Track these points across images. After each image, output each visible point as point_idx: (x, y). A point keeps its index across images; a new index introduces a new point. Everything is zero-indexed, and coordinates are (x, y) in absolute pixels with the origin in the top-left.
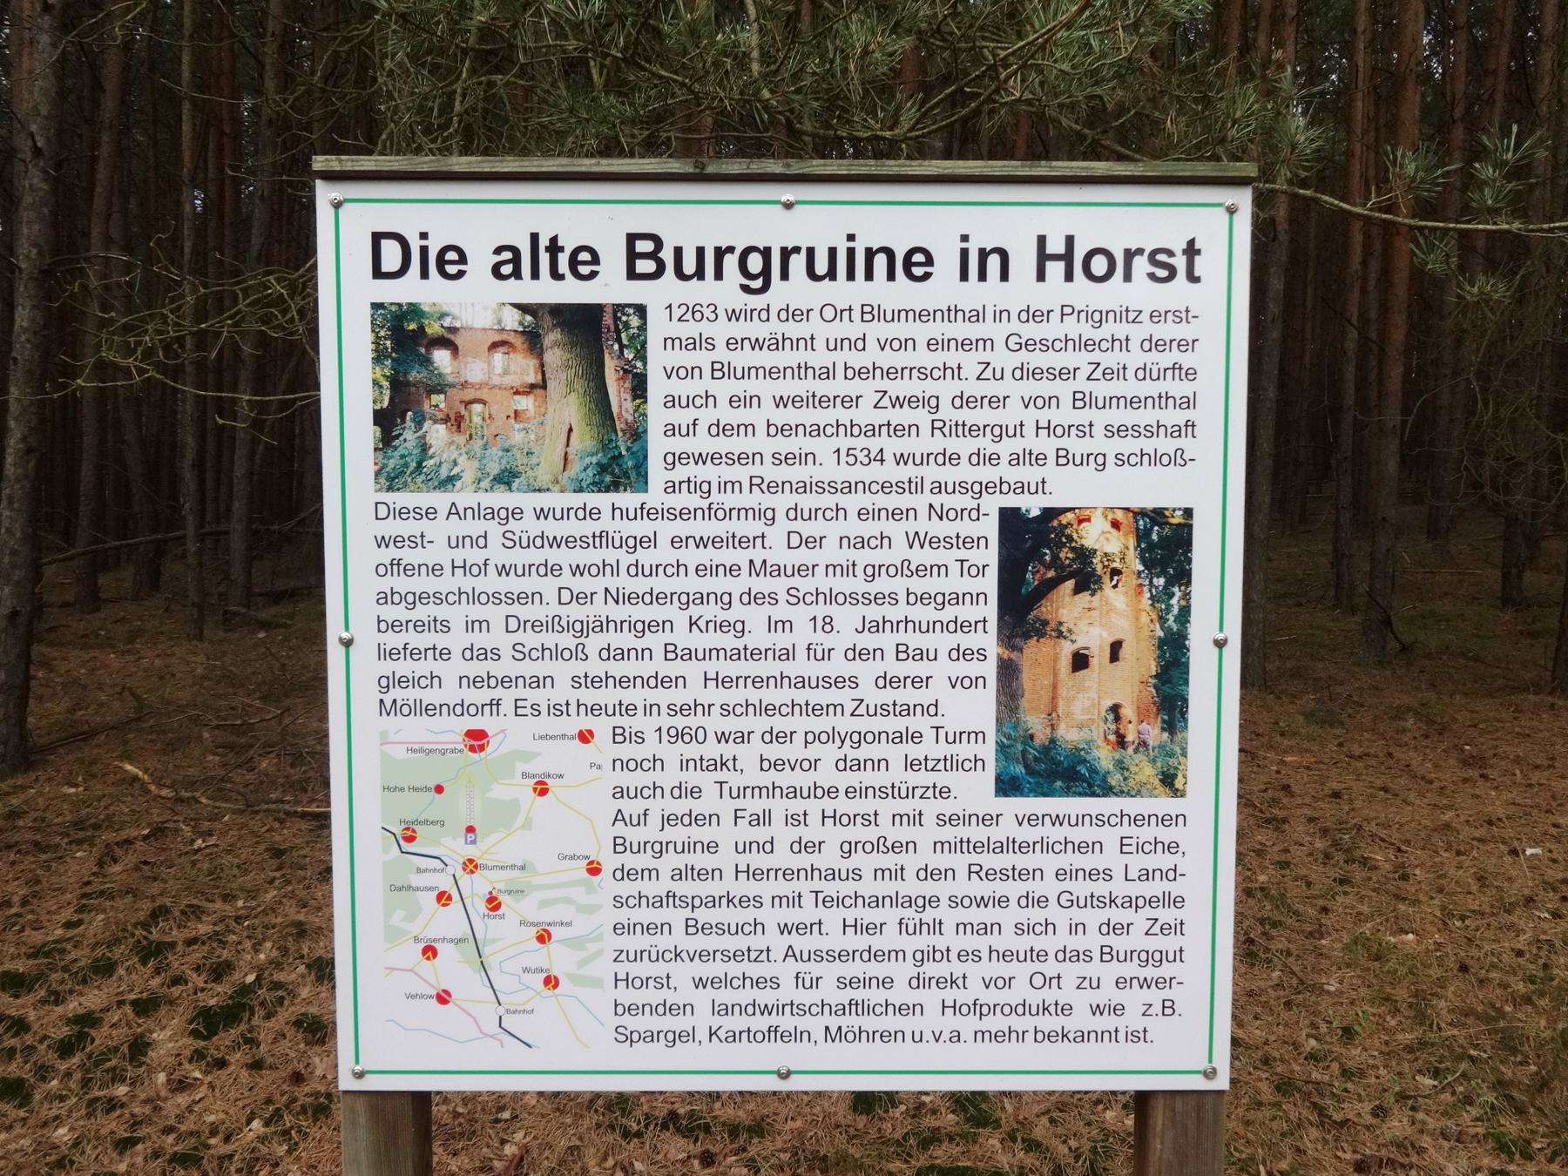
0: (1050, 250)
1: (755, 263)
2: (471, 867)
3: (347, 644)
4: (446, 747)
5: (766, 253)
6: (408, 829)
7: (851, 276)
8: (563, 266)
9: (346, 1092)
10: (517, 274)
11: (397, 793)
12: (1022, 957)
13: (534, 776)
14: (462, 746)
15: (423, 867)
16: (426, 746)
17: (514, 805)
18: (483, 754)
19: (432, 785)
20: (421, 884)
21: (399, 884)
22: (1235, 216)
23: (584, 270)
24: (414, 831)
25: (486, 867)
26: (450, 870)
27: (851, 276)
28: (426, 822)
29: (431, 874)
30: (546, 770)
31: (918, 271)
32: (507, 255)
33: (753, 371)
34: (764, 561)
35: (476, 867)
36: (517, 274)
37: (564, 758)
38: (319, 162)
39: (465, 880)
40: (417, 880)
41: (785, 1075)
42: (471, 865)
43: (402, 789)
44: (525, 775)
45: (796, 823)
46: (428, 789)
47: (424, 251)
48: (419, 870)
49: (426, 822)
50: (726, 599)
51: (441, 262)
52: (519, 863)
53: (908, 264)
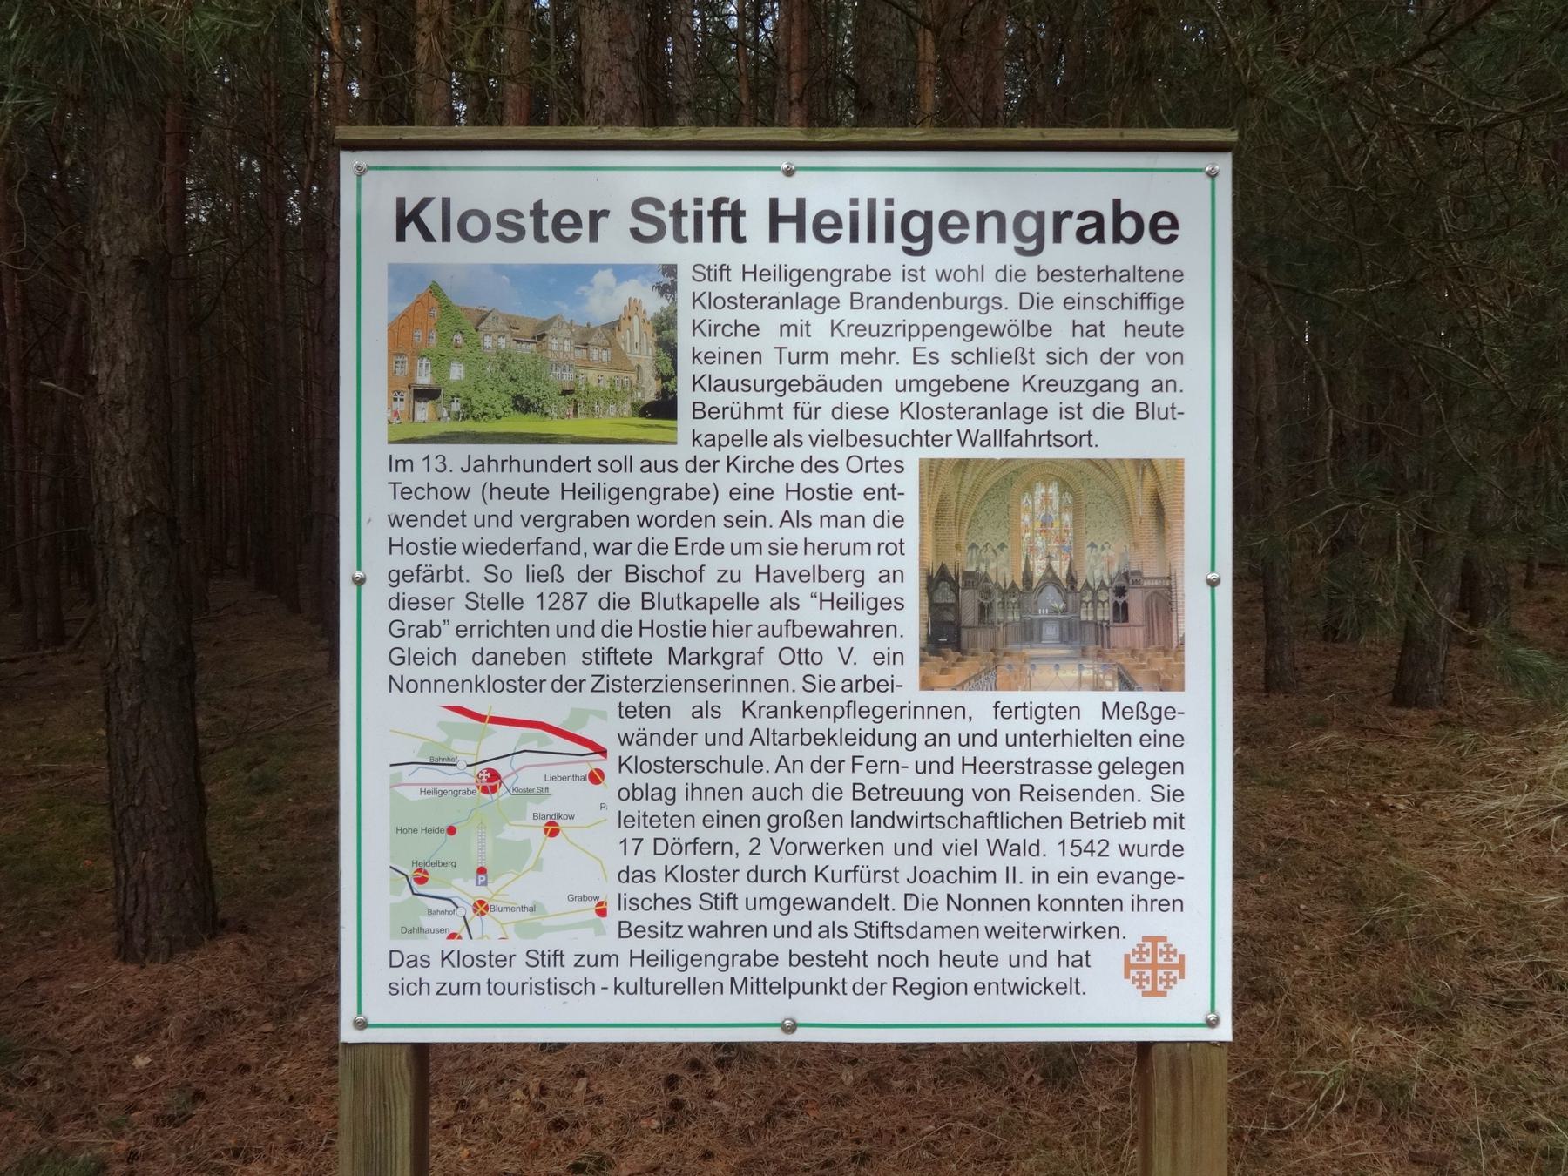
0: (782, 212)
1: (917, 226)
2: (481, 909)
3: (359, 582)
4: (458, 788)
5: (927, 217)
6: (419, 870)
7: (872, 238)
8: (547, 229)
9: (346, 1044)
10: (1100, 237)
11: (410, 835)
12: (972, 962)
13: (545, 817)
14: (475, 788)
15: (434, 909)
16: (440, 788)
17: (525, 846)
18: (495, 795)
19: (445, 826)
20: (432, 926)
21: (410, 926)
22: (1217, 179)
23: (567, 233)
24: (426, 872)
25: (497, 909)
26: (461, 912)
27: (872, 238)
28: (438, 863)
29: (442, 916)
30: (557, 811)
31: (1164, 234)
32: (1091, 220)
33: (914, 384)
34: (684, 649)
35: (486, 908)
36: (1100, 237)
37: (575, 798)
38: (343, 132)
39: (475, 922)
40: (428, 922)
41: (792, 1028)
42: (481, 907)
43: (415, 831)
44: (536, 816)
45: (617, 689)
46: (441, 831)
47: (889, 217)
48: (430, 912)
49: (438, 863)
50: (911, 740)
51: (818, 227)
52: (529, 905)
53: (944, 226)
